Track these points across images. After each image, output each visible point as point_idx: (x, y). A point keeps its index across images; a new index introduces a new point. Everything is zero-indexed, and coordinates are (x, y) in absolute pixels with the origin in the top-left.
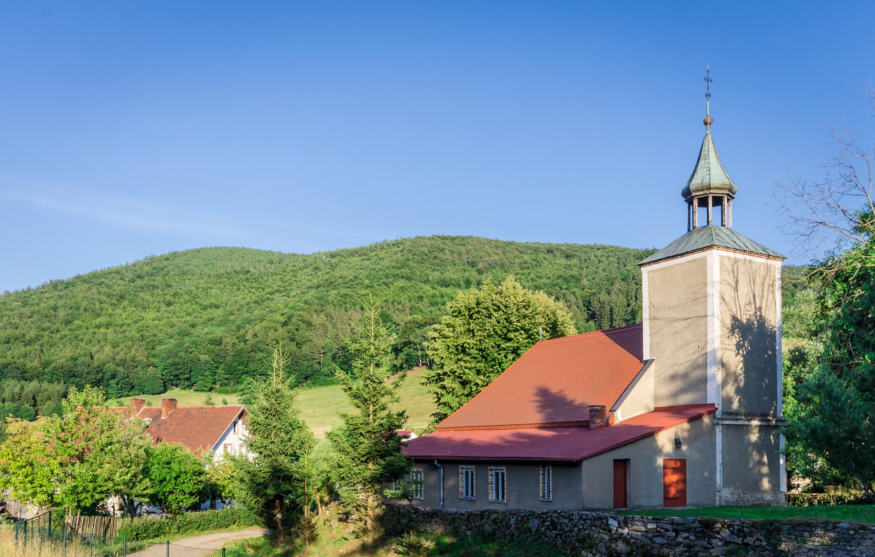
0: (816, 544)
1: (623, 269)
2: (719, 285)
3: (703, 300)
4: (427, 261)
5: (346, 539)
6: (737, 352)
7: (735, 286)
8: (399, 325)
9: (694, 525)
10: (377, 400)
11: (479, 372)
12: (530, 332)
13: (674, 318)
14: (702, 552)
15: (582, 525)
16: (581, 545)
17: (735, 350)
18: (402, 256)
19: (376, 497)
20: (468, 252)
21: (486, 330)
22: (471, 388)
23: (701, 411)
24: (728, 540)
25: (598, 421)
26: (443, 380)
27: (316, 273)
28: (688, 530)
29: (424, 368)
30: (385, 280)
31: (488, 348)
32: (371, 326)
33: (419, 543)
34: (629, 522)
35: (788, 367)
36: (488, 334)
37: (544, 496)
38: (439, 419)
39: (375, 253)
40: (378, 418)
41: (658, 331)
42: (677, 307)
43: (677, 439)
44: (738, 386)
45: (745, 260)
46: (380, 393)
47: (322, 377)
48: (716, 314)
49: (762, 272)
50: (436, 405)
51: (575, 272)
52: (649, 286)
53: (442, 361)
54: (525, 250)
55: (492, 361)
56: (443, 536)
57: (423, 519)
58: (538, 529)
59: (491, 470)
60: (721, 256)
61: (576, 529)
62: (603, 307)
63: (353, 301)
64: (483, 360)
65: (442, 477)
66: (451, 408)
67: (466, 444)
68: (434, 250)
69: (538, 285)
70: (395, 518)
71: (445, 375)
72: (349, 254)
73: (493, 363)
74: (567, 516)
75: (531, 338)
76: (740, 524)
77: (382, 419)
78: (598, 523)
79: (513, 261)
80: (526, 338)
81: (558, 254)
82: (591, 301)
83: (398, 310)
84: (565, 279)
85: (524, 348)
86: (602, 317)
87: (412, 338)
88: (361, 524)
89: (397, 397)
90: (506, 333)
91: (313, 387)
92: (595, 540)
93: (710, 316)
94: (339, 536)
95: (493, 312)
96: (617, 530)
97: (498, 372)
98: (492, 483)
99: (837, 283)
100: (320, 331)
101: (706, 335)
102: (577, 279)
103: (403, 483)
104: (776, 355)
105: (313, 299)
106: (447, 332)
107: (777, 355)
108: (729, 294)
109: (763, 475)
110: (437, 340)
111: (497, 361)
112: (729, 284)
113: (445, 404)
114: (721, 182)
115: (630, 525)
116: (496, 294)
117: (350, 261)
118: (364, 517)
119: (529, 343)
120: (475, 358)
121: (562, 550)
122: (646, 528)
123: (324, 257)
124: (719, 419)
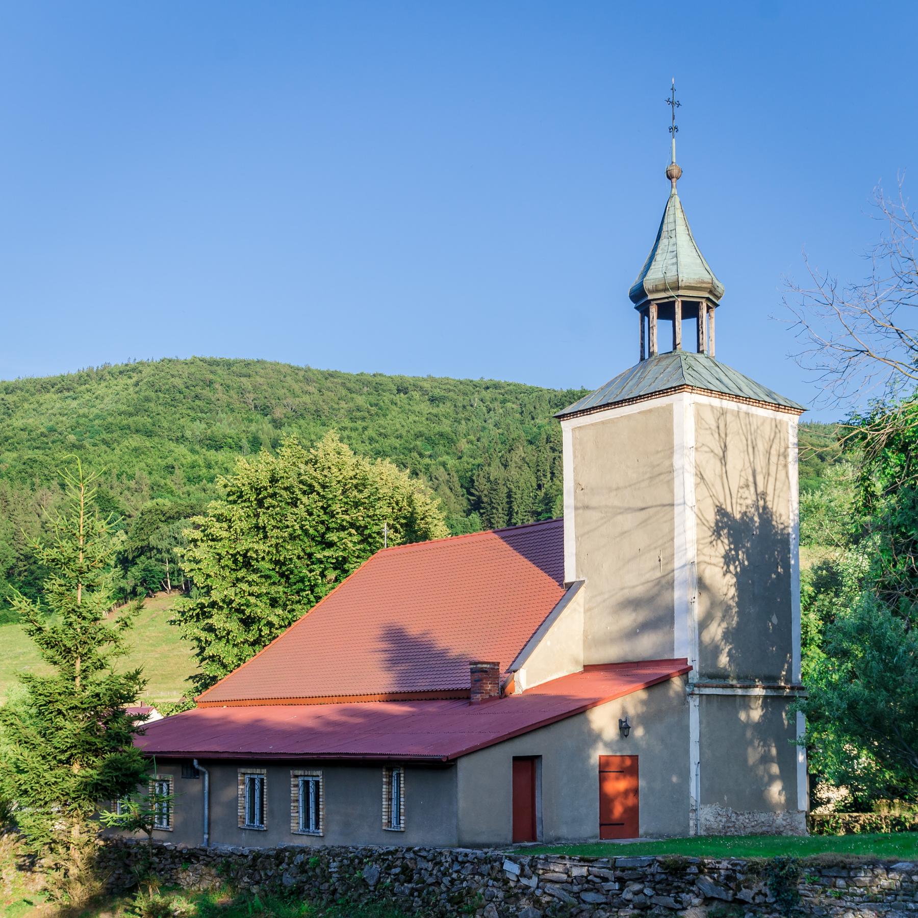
4: (181, 402)
5: (30, 903)
6: (725, 568)
7: (721, 454)
8: (130, 516)
10: (90, 650)
11: (274, 603)
15: (458, 872)
16: (456, 907)
17: (722, 565)
20: (255, 388)
21: (287, 527)
22: (261, 630)
26: (211, 617)
28: (641, 879)
30: (105, 435)
31: (291, 559)
34: (539, 866)
36: (291, 535)
37: (390, 822)
39: (87, 386)
43: (623, 720)
46: (94, 639)
49: (767, 431)
50: (197, 660)
52: (574, 452)
53: (209, 582)
54: (357, 387)
55: (298, 582)
57: (172, 866)
58: (378, 881)
59: (296, 776)
60: (695, 403)
62: (495, 490)
63: (46, 472)
64: (283, 581)
66: (225, 666)
68: (194, 383)
69: (380, 449)
72: (39, 387)
73: (300, 585)
74: (430, 857)
75: (369, 542)
76: (730, 867)
78: (485, 868)
79: (336, 406)
80: (360, 542)
82: (474, 478)
83: (129, 489)
84: (429, 440)
85: (355, 559)
86: (493, 508)
87: (153, 540)
95: (300, 496)
96: (518, 881)
97: (309, 602)
98: (297, 801)
101: (672, 539)
102: (450, 440)
106: (217, 529)
108: (712, 468)
111: (307, 583)
112: (712, 451)
113: (212, 658)
116: (306, 463)
118: (63, 863)
119: (364, 551)
120: (267, 577)
122: (569, 876)
124: (695, 686)
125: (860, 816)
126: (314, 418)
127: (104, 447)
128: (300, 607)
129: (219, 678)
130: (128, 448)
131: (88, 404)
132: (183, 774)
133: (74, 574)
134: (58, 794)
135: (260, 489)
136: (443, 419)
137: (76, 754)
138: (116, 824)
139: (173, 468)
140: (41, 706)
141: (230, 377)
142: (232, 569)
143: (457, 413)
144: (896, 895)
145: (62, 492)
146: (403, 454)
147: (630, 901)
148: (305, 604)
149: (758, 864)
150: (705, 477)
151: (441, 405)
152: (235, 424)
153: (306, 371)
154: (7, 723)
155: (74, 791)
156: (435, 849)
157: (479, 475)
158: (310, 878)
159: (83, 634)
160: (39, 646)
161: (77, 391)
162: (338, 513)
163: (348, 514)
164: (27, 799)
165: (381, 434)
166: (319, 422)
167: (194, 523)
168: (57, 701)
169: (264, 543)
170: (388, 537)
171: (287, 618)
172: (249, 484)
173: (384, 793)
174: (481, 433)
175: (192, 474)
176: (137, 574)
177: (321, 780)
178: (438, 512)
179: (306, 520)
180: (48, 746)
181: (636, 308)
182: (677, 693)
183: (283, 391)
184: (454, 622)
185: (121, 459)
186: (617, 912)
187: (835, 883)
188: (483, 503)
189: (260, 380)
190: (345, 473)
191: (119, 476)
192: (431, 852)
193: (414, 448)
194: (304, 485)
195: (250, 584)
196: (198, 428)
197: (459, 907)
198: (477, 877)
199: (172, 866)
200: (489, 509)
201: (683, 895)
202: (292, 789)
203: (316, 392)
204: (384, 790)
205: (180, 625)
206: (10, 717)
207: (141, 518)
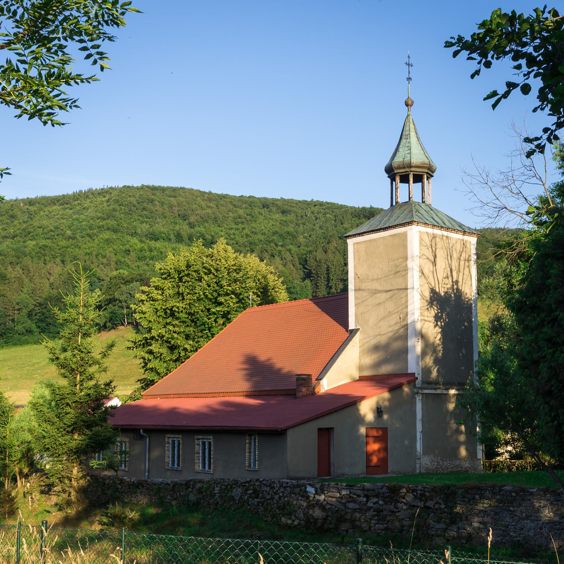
0: (485, 505)
1: (340, 227)
2: (418, 259)
3: (404, 273)
4: (135, 212)
5: (49, 512)
6: (435, 323)
7: (433, 260)
8: (103, 280)
9: (383, 490)
10: (85, 370)
11: (187, 337)
12: (241, 297)
13: (377, 290)
14: (390, 516)
15: (282, 492)
16: (281, 512)
17: (434, 321)
18: (108, 206)
19: (81, 468)
20: (179, 204)
21: (196, 293)
22: (180, 353)
23: (403, 380)
24: (413, 504)
25: (304, 390)
26: (151, 345)
27: (12, 222)
28: (377, 496)
29: (130, 327)
30: (89, 231)
31: (198, 312)
32: (80, 296)
33: (123, 513)
34: (325, 489)
35: (488, 336)
36: (198, 298)
37: (250, 465)
38: (145, 385)
39: (79, 201)
40: (86, 388)
41: (362, 302)
42: (380, 279)
43: (379, 407)
44: (436, 356)
45: (443, 236)
46: (87, 363)
47: (16, 336)
48: (415, 287)
49: (459, 247)
50: (143, 370)
51: (291, 228)
52: (354, 257)
53: (150, 325)
54: (239, 204)
55: (201, 325)
56: (148, 506)
57: (129, 490)
58: (241, 498)
59: (198, 439)
60: (420, 232)
61: (277, 497)
62: (319, 266)
63: (53, 253)
64: (193, 324)
65: (147, 446)
66: (159, 374)
67: (173, 412)
68: (143, 201)
69: (253, 241)
70: (100, 489)
71: (152, 340)
72: (49, 202)
73: (203, 327)
74: (268, 484)
75: (243, 304)
76: (422, 489)
77: (90, 389)
78: (297, 490)
79: (226, 215)
80: (237, 303)
81: (274, 209)
82: (307, 259)
83: (102, 264)
84: (281, 236)
85: (234, 312)
86: (318, 277)
87: (117, 295)
88: (65, 496)
89: (105, 366)
90: (216, 298)
91: (5, 347)
92: (294, 507)
93: (410, 288)
94: (40, 509)
95: (203, 276)
96: (314, 497)
97: (208, 337)
98: (199, 453)
99: (520, 263)
100: (15, 286)
101: (407, 307)
102: (293, 236)
103: (108, 453)
104: (472, 327)
105: (9, 250)
106: (156, 294)
107: (474, 326)
108: (428, 268)
109: (460, 444)
110: (145, 302)
111: (207, 326)
112: (428, 258)
113: (151, 369)
114: (421, 161)
115: (326, 492)
116: (207, 257)
117: (51, 210)
118: (67, 489)
119: (240, 307)
120: (184, 322)
121: (264, 517)
122: (340, 494)
123: (22, 205)
124: (419, 388)
125: (516, 462)
126: (213, 222)
127: (88, 239)
128: (202, 340)
129: (155, 381)
130: (102, 239)
131: (78, 213)
132: (134, 437)
133: (77, 328)
134: (66, 450)
135: (180, 271)
136: (289, 223)
137: (76, 428)
138: (98, 467)
139: (129, 251)
140: (57, 401)
141: (164, 197)
142: (163, 318)
143: (298, 220)
144: (504, 503)
145: (62, 265)
146: (266, 244)
147: (371, 507)
148: (205, 338)
149: (436, 487)
150: (424, 272)
151: (288, 215)
152: (167, 225)
153: (209, 194)
154: (38, 410)
155: (75, 448)
156: (271, 480)
157: (310, 257)
158: (204, 496)
159: (81, 361)
160: (56, 367)
161: (72, 204)
162: (225, 286)
163: (230, 286)
164: (48, 453)
165: (253, 232)
166: (216, 225)
167: (142, 290)
168: (66, 398)
169: (182, 302)
170: (253, 300)
171: (195, 346)
172: (174, 268)
173: (247, 449)
174: (312, 232)
175: (140, 254)
176: (107, 315)
177: (212, 441)
178: (282, 285)
179: (206, 289)
180: (61, 423)
181: (388, 177)
182: (407, 394)
183: (195, 206)
184: (288, 351)
185: (98, 245)
186: (365, 513)
187: (474, 497)
188: (312, 274)
189: (182, 199)
190: (229, 263)
191: (97, 256)
192: (269, 481)
193: (272, 241)
194: (205, 269)
195: (174, 326)
196: (145, 227)
197: (283, 512)
198: (292, 495)
199: (129, 490)
200: (316, 277)
201: (399, 504)
202: (196, 446)
203: (215, 207)
204: (247, 447)
205: (133, 350)
206: (40, 407)
207: (109, 281)
